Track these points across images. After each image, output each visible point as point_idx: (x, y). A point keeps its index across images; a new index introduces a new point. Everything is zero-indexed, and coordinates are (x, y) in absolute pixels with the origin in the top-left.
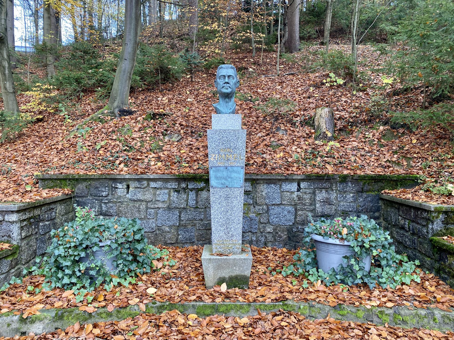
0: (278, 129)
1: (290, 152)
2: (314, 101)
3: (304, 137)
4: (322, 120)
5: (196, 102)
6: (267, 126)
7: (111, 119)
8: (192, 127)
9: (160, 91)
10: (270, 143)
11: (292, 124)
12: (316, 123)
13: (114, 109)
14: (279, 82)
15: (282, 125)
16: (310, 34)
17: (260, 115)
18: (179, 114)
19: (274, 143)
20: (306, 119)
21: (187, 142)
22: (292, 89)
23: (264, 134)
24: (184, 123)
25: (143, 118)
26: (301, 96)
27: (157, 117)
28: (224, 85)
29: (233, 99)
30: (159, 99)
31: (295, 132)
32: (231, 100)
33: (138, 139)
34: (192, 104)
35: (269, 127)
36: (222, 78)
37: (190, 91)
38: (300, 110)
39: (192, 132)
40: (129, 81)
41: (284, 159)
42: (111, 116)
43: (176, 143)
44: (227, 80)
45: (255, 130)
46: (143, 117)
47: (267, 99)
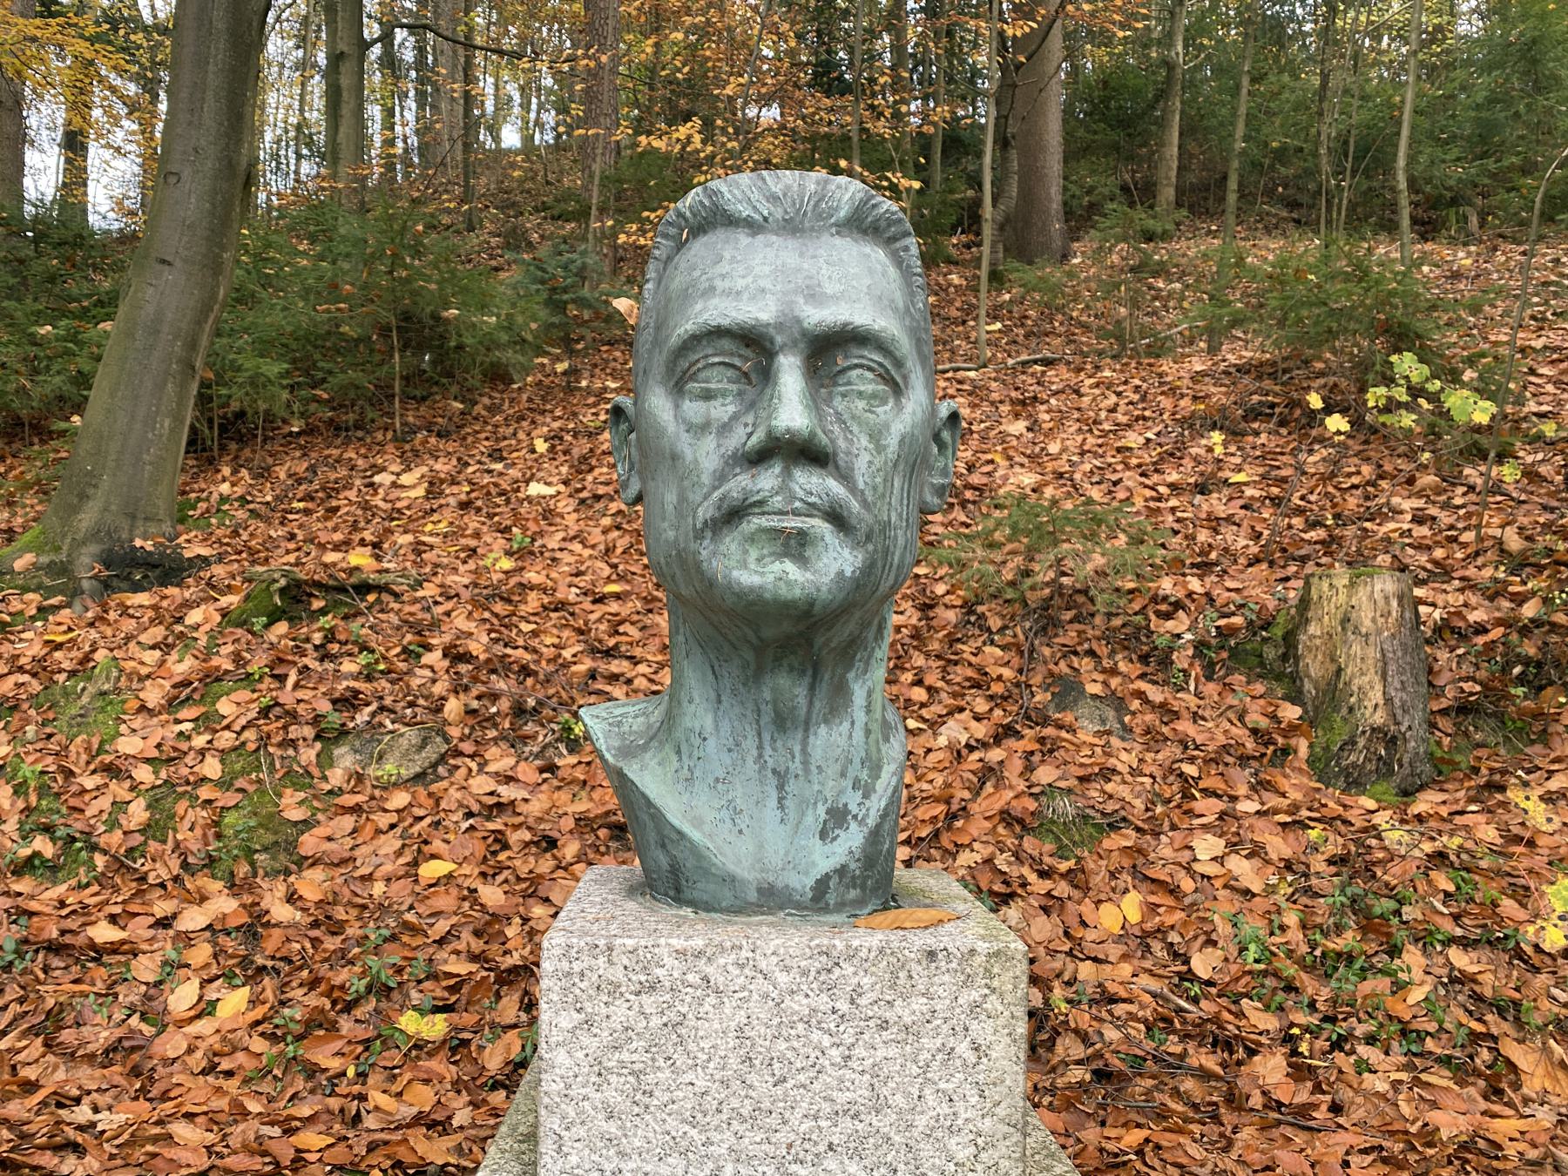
0: (1067, 690)
1: (1187, 885)
2: (1234, 508)
3: (1244, 760)
4: (1356, 648)
5: (573, 503)
6: (994, 671)
7: (43, 611)
8: (525, 671)
9: (395, 439)
10: (1032, 805)
11: (1144, 659)
12: (1314, 667)
13: (77, 544)
14: (1013, 402)
15: (1086, 664)
16: (1093, 198)
17: (940, 589)
18: (459, 580)
19: (1066, 807)
20: (1232, 631)
21: (481, 785)
22: (1091, 441)
23: (981, 730)
24: (478, 646)
25: (225, 613)
26: (1156, 478)
27: (317, 604)
28: (741, 483)
29: (868, 684)
30: (383, 479)
31: (1176, 715)
32: (841, 692)
33: (144, 774)
34: (549, 515)
35: (1007, 673)
36: (717, 380)
37: (554, 438)
38: (1176, 566)
39: (519, 711)
40: (183, 386)
41: (1157, 946)
42: (51, 592)
43: (400, 799)
44: (791, 409)
45: (919, 694)
46: (224, 601)
47: (969, 494)
